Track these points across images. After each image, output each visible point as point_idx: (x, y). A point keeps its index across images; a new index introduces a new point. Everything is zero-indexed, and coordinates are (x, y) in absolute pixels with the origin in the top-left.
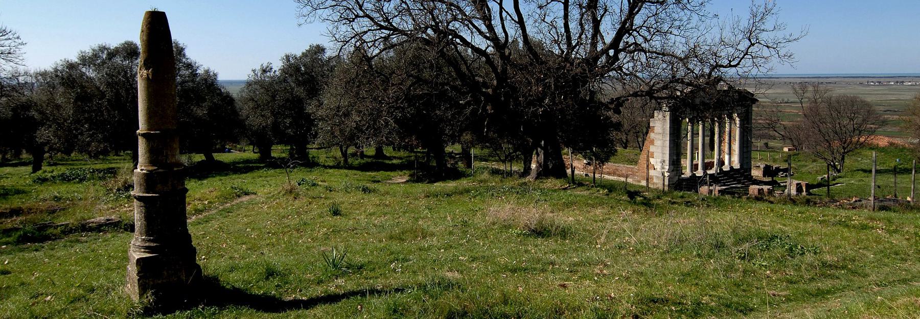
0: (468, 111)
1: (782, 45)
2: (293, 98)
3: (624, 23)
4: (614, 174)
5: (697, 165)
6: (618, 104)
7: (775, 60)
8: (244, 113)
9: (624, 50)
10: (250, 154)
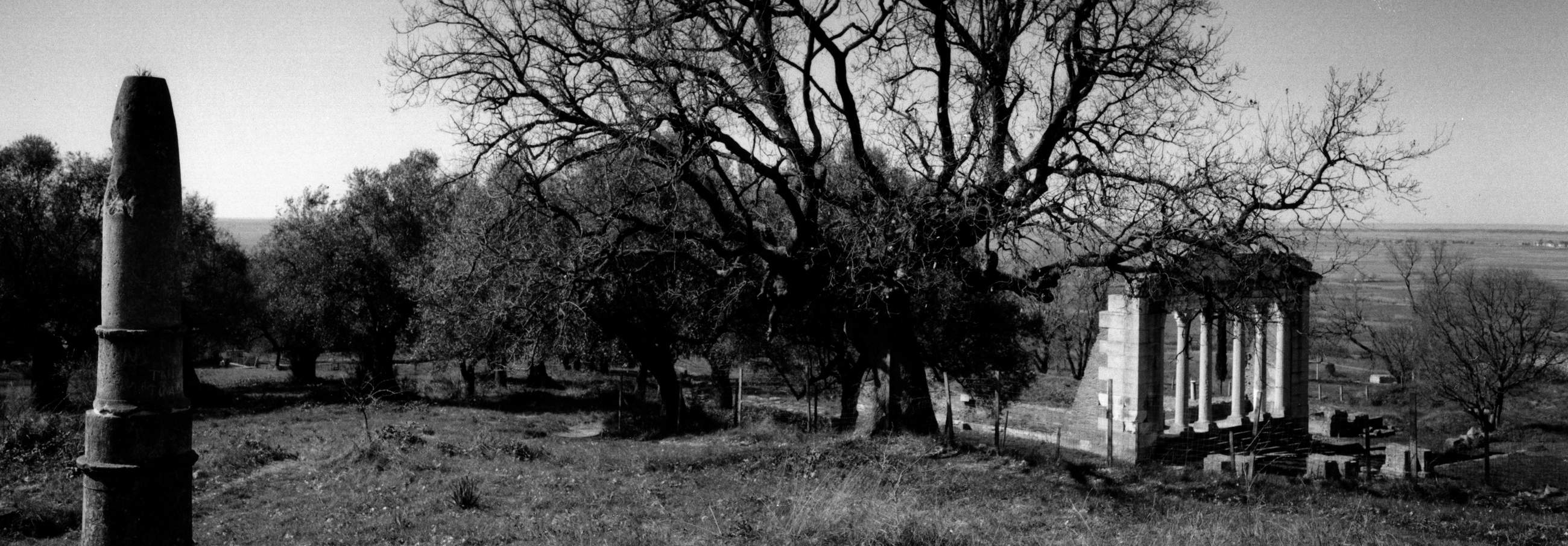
0: (736, 291)
1: (1394, 164)
2: (370, 258)
3: (1063, 112)
4: (1023, 424)
5: (1195, 410)
6: (1046, 280)
7: (1380, 193)
8: (270, 285)
9: (1059, 169)
10: (271, 371)
